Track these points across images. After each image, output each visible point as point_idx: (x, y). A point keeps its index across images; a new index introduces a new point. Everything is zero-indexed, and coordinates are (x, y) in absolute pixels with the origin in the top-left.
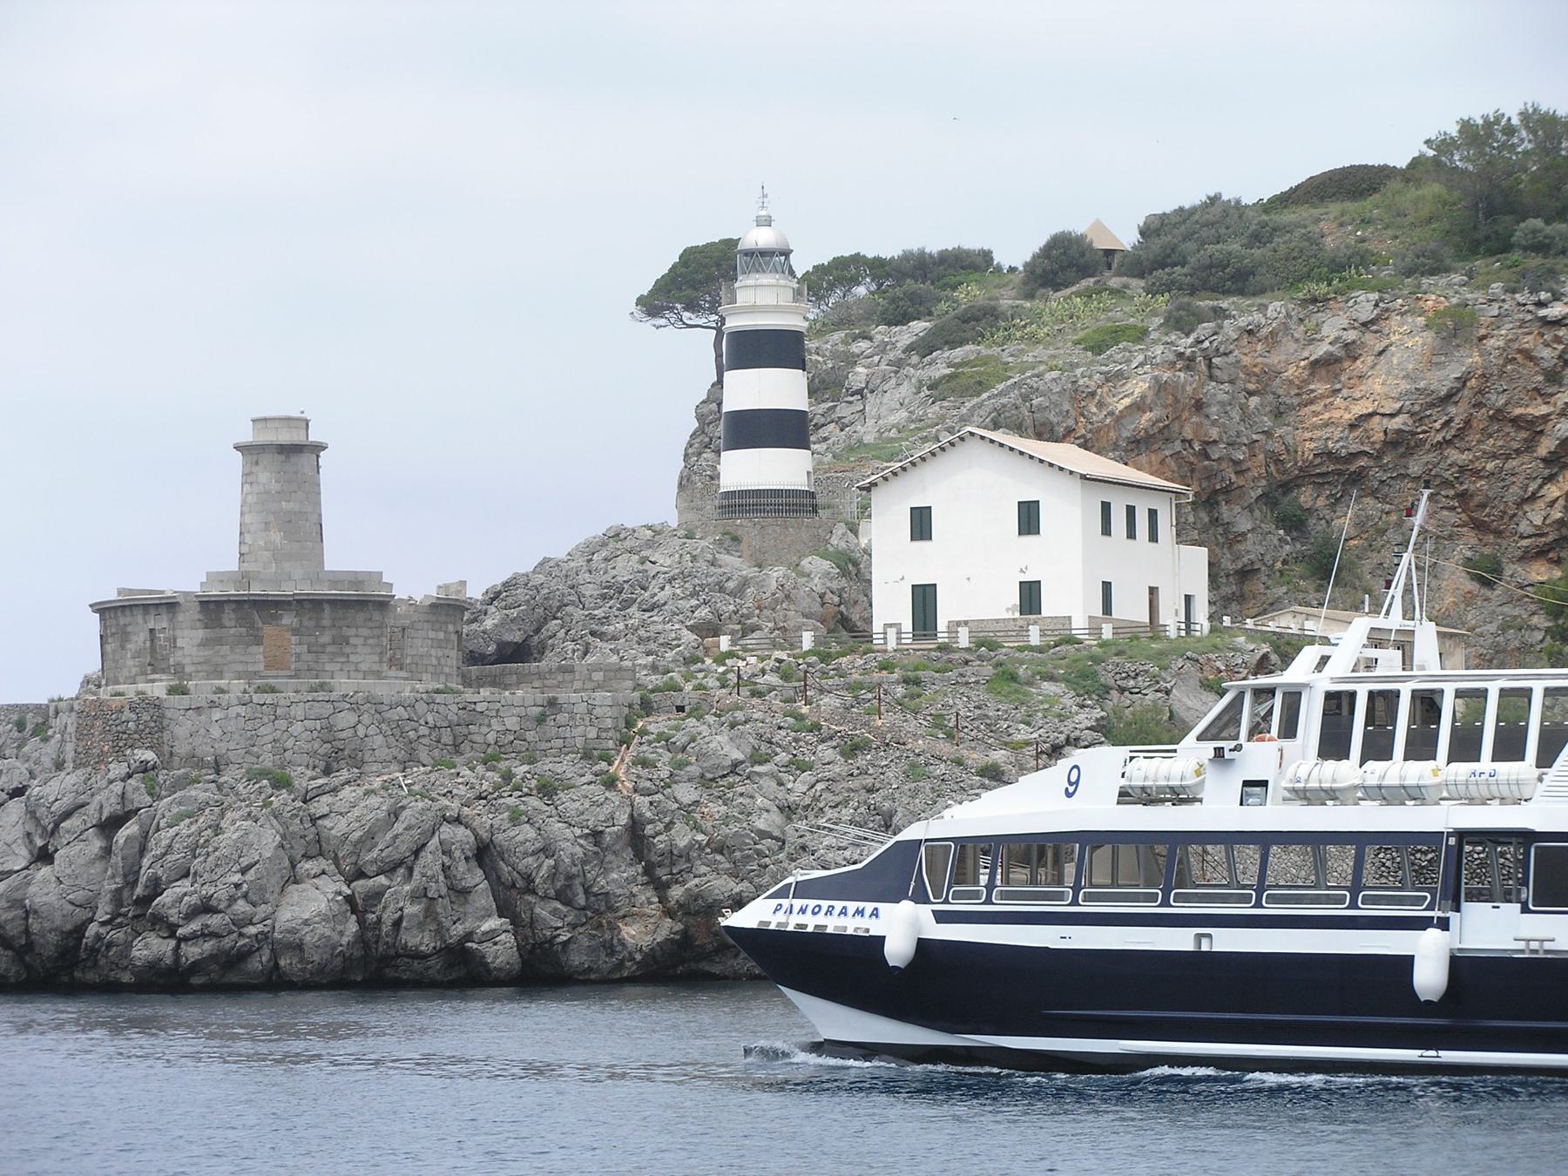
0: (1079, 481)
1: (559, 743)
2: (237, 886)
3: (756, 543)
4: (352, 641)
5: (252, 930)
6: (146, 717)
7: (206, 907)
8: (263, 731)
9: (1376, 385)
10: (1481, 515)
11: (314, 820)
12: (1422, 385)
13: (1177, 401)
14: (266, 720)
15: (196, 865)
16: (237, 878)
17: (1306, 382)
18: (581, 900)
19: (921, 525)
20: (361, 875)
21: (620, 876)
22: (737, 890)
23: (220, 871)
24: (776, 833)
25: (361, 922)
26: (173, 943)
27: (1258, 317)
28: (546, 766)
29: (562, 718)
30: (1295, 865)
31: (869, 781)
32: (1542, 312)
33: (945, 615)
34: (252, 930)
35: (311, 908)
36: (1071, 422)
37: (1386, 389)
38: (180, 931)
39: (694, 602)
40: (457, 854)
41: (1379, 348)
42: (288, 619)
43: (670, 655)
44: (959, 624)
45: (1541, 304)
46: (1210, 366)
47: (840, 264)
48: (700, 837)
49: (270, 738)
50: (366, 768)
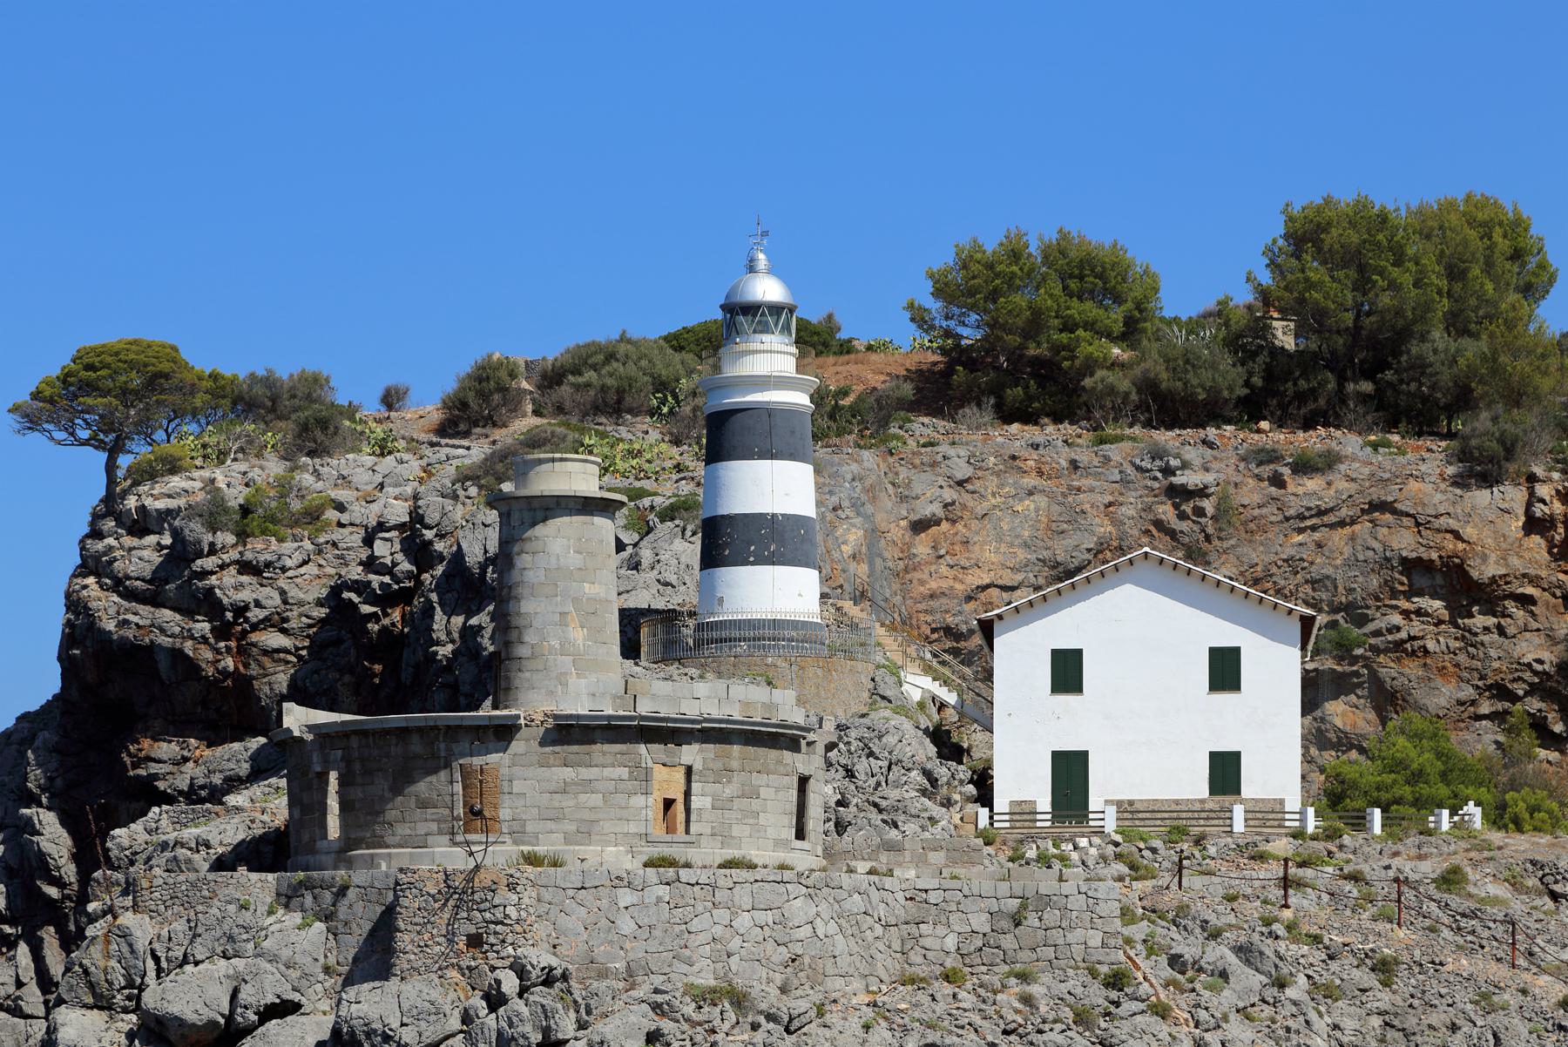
1: (1049, 952)
4: (763, 792)
8: (694, 926)
12: (1046, 554)
14: (700, 909)
17: (909, 545)
19: (1067, 671)
29: (1051, 916)
41: (980, 511)
45: (1168, 471)
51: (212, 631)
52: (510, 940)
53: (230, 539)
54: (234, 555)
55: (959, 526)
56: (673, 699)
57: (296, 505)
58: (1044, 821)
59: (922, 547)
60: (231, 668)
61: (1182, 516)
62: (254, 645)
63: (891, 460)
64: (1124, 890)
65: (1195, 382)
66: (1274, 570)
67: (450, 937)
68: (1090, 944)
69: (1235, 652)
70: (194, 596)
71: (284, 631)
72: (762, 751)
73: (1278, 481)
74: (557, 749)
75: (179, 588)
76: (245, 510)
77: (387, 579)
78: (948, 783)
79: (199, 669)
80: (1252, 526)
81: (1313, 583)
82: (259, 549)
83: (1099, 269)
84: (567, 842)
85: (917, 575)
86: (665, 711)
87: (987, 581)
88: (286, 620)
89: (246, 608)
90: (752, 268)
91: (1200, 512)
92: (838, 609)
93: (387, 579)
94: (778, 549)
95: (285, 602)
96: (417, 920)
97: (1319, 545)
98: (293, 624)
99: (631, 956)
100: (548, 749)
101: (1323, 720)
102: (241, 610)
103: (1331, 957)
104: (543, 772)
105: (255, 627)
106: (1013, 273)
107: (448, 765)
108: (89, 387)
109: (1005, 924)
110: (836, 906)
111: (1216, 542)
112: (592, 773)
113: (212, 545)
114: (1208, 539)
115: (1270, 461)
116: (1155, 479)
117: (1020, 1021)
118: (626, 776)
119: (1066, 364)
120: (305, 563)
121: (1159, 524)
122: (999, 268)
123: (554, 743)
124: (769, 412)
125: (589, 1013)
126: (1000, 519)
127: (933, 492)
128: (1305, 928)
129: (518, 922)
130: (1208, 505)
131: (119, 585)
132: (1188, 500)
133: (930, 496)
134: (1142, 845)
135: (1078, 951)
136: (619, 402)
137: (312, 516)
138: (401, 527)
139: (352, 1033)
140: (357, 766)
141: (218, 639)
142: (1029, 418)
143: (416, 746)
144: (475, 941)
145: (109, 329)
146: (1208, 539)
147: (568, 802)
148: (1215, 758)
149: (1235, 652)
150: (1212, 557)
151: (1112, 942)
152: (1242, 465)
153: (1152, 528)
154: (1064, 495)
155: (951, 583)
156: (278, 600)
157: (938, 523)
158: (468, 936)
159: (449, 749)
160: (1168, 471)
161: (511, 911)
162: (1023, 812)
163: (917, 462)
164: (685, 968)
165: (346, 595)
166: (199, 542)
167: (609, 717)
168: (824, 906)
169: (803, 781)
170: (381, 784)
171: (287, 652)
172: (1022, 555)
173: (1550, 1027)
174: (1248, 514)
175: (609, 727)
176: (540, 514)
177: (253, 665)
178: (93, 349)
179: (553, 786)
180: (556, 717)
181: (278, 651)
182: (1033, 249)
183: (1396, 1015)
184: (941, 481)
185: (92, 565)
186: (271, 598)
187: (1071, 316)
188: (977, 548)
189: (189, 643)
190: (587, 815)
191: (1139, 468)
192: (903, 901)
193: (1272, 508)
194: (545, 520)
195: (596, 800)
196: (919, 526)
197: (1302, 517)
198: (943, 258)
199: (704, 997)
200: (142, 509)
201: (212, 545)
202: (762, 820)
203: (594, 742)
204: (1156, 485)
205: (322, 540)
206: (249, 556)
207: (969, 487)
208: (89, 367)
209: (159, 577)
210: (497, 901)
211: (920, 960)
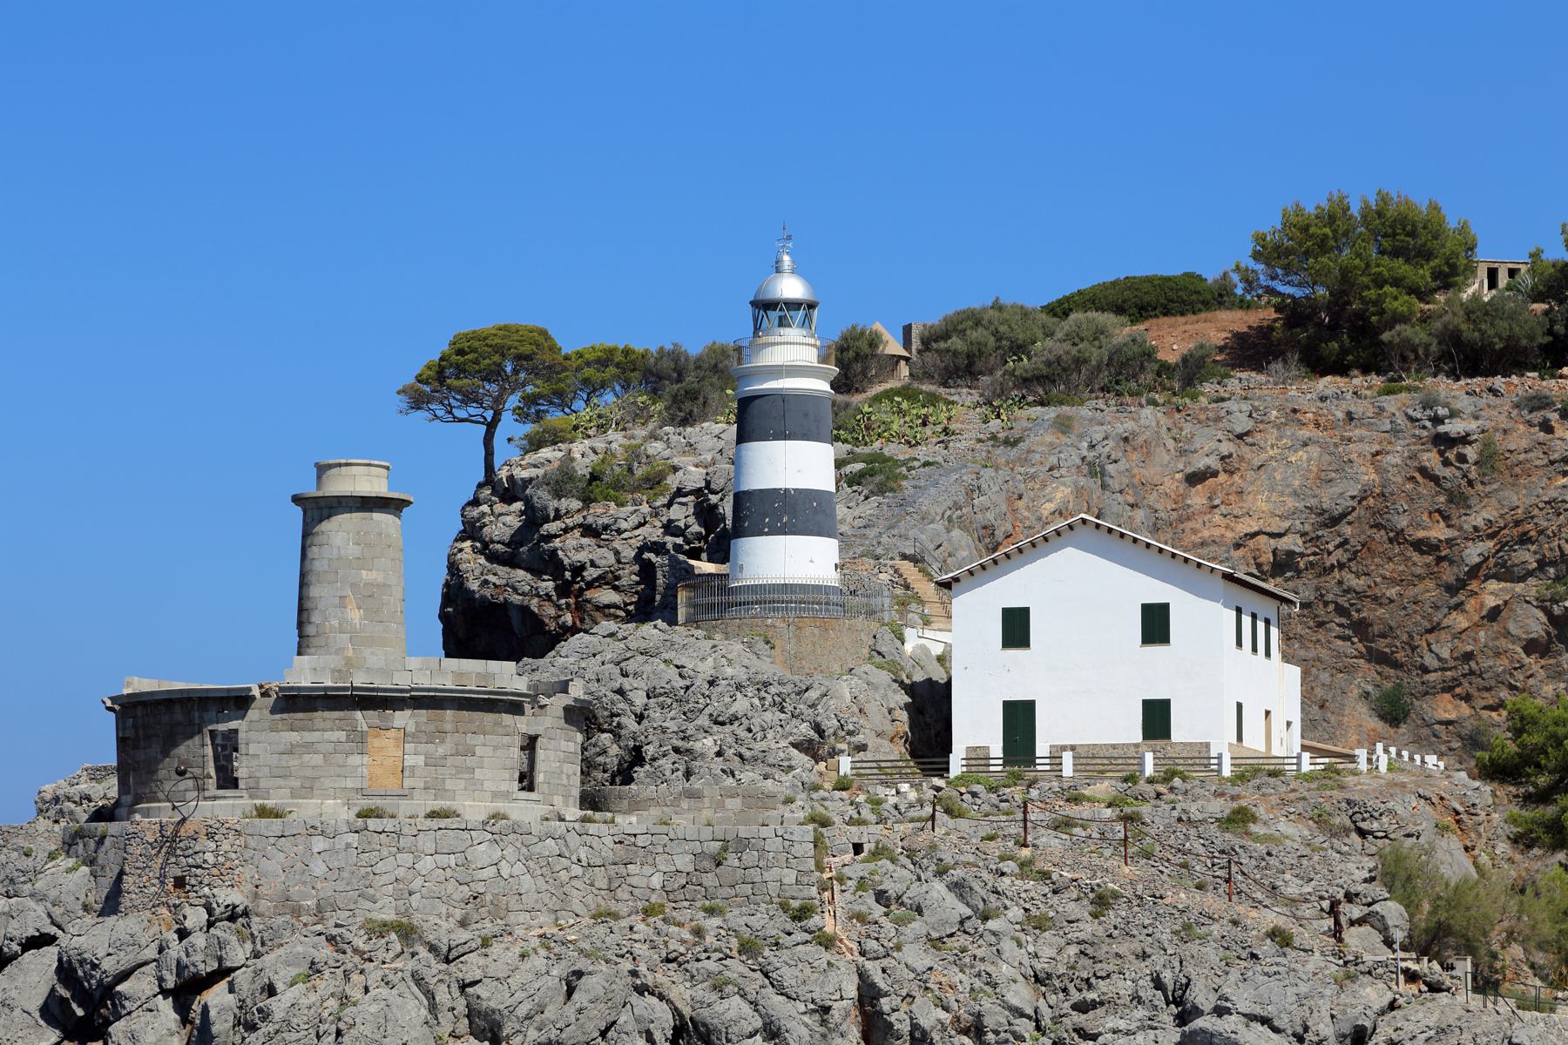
0: (1221, 582)
1: (748, 889)
3: (791, 647)
4: (478, 751)
8: (380, 867)
10: (1381, 645)
11: (463, 987)
12: (1312, 502)
17: (1184, 496)
19: (1016, 628)
27: (1130, 425)
29: (750, 857)
37: (1271, 506)
41: (1257, 463)
42: (403, 718)
44: (1064, 748)
45: (1437, 420)
49: (390, 878)
50: (512, 918)
51: (556, 588)
52: (206, 881)
53: (576, 504)
54: (578, 519)
55: (1236, 477)
56: (388, 673)
57: (639, 472)
58: (996, 767)
59: (1197, 498)
60: (570, 623)
62: (588, 601)
63: (1177, 416)
64: (886, 832)
65: (1491, 332)
66: (1536, 512)
67: (162, 879)
68: (786, 881)
70: (541, 558)
71: (616, 588)
72: (477, 715)
73: (1547, 427)
74: (285, 716)
75: (530, 550)
76: (594, 477)
77: (680, 541)
78: (835, 734)
79: (543, 624)
80: (1517, 470)
82: (600, 513)
83: (1409, 228)
84: (293, 796)
85: (1189, 525)
86: (380, 682)
87: (1256, 529)
88: (618, 578)
89: (583, 567)
90: (778, 270)
91: (1462, 458)
92: (896, 571)
93: (680, 541)
94: (790, 520)
95: (619, 562)
96: (139, 864)
98: (624, 582)
99: (322, 894)
100: (278, 716)
102: (578, 570)
103: (1055, 892)
104: (274, 736)
105: (590, 585)
106: (1326, 236)
107: (200, 732)
108: (461, 371)
109: (707, 864)
110: (524, 850)
111: (1479, 487)
113: (557, 510)
114: (1470, 483)
115: (1540, 408)
116: (1424, 427)
117: (682, 950)
118: (343, 739)
119: (1374, 319)
120: (641, 525)
121: (1423, 471)
122: (1312, 230)
123: (282, 711)
124: (783, 397)
125: (263, 944)
126: (1275, 470)
128: (1040, 865)
129: (214, 866)
130: (1471, 452)
131: (485, 549)
132: (1452, 447)
134: (963, 790)
135: (773, 888)
136: (971, 364)
137: (654, 482)
138: (697, 492)
139: (69, 962)
140: (141, 732)
141: (560, 597)
142: (1341, 370)
143: (179, 716)
144: (180, 883)
145: (482, 317)
146: (1470, 483)
147: (293, 762)
148: (1148, 705)
150: (1472, 502)
151: (805, 879)
152: (1515, 413)
153: (1417, 475)
154: (1336, 445)
155: (1223, 531)
156: (612, 559)
157: (1215, 474)
158: (176, 878)
159: (201, 717)
160: (1437, 420)
161: (210, 857)
162: (978, 757)
163: (1203, 417)
164: (369, 905)
165: (646, 555)
166: (546, 508)
167: (326, 689)
168: (509, 850)
169: (530, 744)
170: (155, 749)
171: (617, 607)
172: (1291, 503)
173: (1244, 956)
174: (1514, 458)
175: (326, 697)
176: (325, 512)
177: (587, 620)
178: (466, 335)
179: (282, 748)
180: (281, 689)
181: (608, 606)
182: (1355, 210)
183: (1092, 944)
184: (1220, 435)
185: (471, 531)
186: (605, 558)
187: (1380, 274)
188: (1251, 497)
189: (535, 600)
190: (309, 773)
191: (1412, 419)
192: (612, 845)
193: (1538, 453)
194: (329, 517)
195: (317, 759)
196: (1194, 479)
198: (1270, 223)
199: (378, 930)
200: (511, 478)
201: (557, 510)
202: (478, 774)
203: (316, 710)
204: (1425, 433)
205: (658, 504)
206: (590, 520)
207: (1249, 440)
208: (461, 352)
209: (516, 540)
210: (197, 849)
211: (626, 896)
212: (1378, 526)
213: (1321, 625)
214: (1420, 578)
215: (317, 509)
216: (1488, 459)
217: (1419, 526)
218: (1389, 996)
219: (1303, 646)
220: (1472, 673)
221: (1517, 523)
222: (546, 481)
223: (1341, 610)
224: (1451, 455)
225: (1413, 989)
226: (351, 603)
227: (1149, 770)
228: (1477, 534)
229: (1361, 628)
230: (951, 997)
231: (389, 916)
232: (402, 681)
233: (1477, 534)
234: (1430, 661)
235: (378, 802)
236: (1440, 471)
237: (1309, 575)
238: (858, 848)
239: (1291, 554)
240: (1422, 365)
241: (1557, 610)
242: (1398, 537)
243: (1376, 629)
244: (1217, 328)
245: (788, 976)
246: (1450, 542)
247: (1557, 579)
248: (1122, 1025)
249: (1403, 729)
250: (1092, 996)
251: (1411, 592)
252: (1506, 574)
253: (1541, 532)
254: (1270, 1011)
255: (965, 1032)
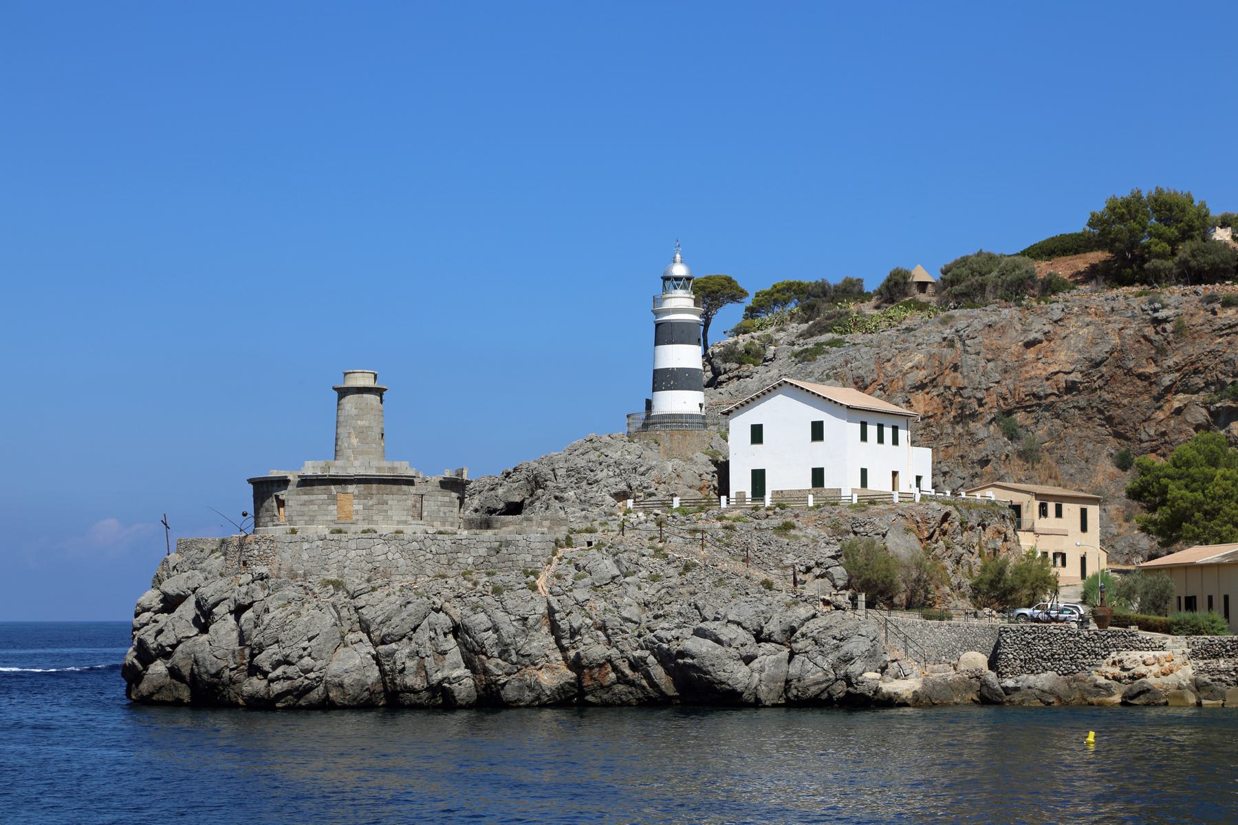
2: (305, 649)
5: (312, 675)
6: (264, 547)
7: (286, 662)
8: (331, 556)
9: (1062, 356)
10: (1120, 429)
11: (357, 609)
12: (1087, 355)
13: (941, 364)
15: (282, 636)
16: (306, 644)
17: (1023, 354)
18: (514, 658)
19: (757, 434)
20: (383, 642)
21: (541, 642)
22: (608, 653)
23: (295, 640)
24: (635, 619)
25: (382, 671)
26: (265, 682)
27: (994, 318)
28: (499, 578)
29: (512, 549)
30: (955, 640)
31: (692, 589)
32: (1156, 315)
33: (771, 486)
34: (312, 675)
35: (352, 664)
36: (875, 376)
38: (270, 675)
39: (618, 479)
40: (438, 631)
42: (352, 488)
43: (596, 510)
45: (1156, 310)
46: (964, 344)
47: (777, 290)
48: (588, 621)
50: (393, 578)
56: (345, 468)
58: (749, 502)
59: (1030, 355)
61: (1157, 333)
69: (821, 423)
72: (389, 486)
73: (1214, 313)
81: (1225, 362)
91: (1164, 330)
97: (1230, 343)
101: (1229, 432)
111: (1173, 345)
112: (314, 497)
114: (1169, 343)
121: (1145, 337)
127: (1038, 327)
130: (1169, 327)
133: (1038, 327)
135: (521, 563)
142: (1130, 283)
146: (1169, 343)
147: (306, 509)
148: (814, 470)
149: (821, 423)
157: (1041, 342)
162: (741, 496)
172: (1077, 356)
174: (1194, 329)
191: (1143, 310)
195: (315, 507)
196: (1029, 345)
197: (1221, 329)
199: (326, 583)
202: (390, 513)
212: (1119, 367)
213: (1090, 419)
214: (1141, 393)
215: (343, 392)
216: (1180, 331)
217: (1140, 366)
218: (813, 612)
219: (1081, 430)
220: (1166, 442)
221: (1192, 363)
222: (720, 354)
223: (1100, 411)
224: (1159, 329)
225: (828, 608)
226: (353, 436)
227: (811, 504)
228: (1170, 370)
229: (1109, 420)
230: (593, 613)
231: (334, 577)
232: (352, 472)
233: (1170, 370)
234: (1144, 436)
235: (341, 526)
236: (1154, 337)
237: (1085, 393)
238: (590, 544)
239: (1074, 383)
240: (1168, 279)
241: (1212, 408)
242: (1129, 372)
243: (1116, 421)
244: (1082, 262)
245: (510, 604)
246: (1156, 374)
247: (1216, 392)
248: (666, 625)
249: (1129, 472)
250: (661, 612)
251: (1135, 401)
252: (1187, 390)
253: (1206, 368)
254: (741, 619)
255: (599, 629)
